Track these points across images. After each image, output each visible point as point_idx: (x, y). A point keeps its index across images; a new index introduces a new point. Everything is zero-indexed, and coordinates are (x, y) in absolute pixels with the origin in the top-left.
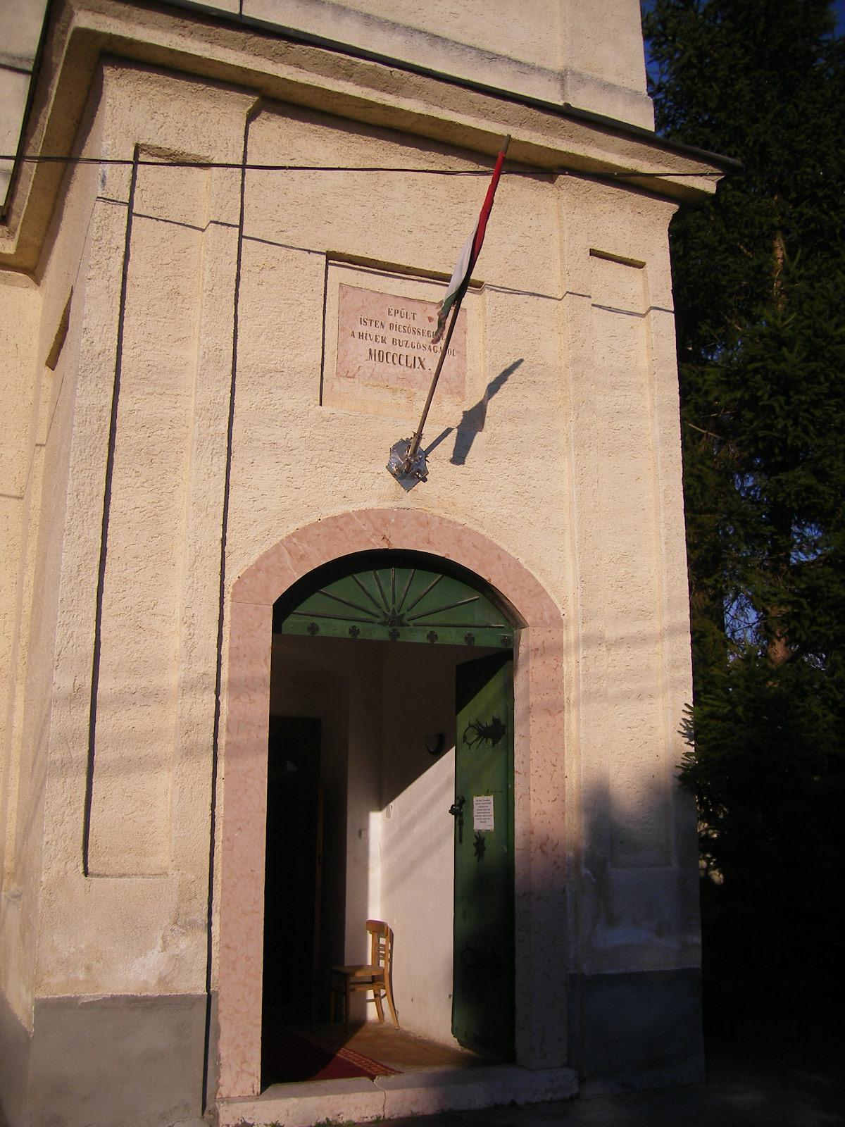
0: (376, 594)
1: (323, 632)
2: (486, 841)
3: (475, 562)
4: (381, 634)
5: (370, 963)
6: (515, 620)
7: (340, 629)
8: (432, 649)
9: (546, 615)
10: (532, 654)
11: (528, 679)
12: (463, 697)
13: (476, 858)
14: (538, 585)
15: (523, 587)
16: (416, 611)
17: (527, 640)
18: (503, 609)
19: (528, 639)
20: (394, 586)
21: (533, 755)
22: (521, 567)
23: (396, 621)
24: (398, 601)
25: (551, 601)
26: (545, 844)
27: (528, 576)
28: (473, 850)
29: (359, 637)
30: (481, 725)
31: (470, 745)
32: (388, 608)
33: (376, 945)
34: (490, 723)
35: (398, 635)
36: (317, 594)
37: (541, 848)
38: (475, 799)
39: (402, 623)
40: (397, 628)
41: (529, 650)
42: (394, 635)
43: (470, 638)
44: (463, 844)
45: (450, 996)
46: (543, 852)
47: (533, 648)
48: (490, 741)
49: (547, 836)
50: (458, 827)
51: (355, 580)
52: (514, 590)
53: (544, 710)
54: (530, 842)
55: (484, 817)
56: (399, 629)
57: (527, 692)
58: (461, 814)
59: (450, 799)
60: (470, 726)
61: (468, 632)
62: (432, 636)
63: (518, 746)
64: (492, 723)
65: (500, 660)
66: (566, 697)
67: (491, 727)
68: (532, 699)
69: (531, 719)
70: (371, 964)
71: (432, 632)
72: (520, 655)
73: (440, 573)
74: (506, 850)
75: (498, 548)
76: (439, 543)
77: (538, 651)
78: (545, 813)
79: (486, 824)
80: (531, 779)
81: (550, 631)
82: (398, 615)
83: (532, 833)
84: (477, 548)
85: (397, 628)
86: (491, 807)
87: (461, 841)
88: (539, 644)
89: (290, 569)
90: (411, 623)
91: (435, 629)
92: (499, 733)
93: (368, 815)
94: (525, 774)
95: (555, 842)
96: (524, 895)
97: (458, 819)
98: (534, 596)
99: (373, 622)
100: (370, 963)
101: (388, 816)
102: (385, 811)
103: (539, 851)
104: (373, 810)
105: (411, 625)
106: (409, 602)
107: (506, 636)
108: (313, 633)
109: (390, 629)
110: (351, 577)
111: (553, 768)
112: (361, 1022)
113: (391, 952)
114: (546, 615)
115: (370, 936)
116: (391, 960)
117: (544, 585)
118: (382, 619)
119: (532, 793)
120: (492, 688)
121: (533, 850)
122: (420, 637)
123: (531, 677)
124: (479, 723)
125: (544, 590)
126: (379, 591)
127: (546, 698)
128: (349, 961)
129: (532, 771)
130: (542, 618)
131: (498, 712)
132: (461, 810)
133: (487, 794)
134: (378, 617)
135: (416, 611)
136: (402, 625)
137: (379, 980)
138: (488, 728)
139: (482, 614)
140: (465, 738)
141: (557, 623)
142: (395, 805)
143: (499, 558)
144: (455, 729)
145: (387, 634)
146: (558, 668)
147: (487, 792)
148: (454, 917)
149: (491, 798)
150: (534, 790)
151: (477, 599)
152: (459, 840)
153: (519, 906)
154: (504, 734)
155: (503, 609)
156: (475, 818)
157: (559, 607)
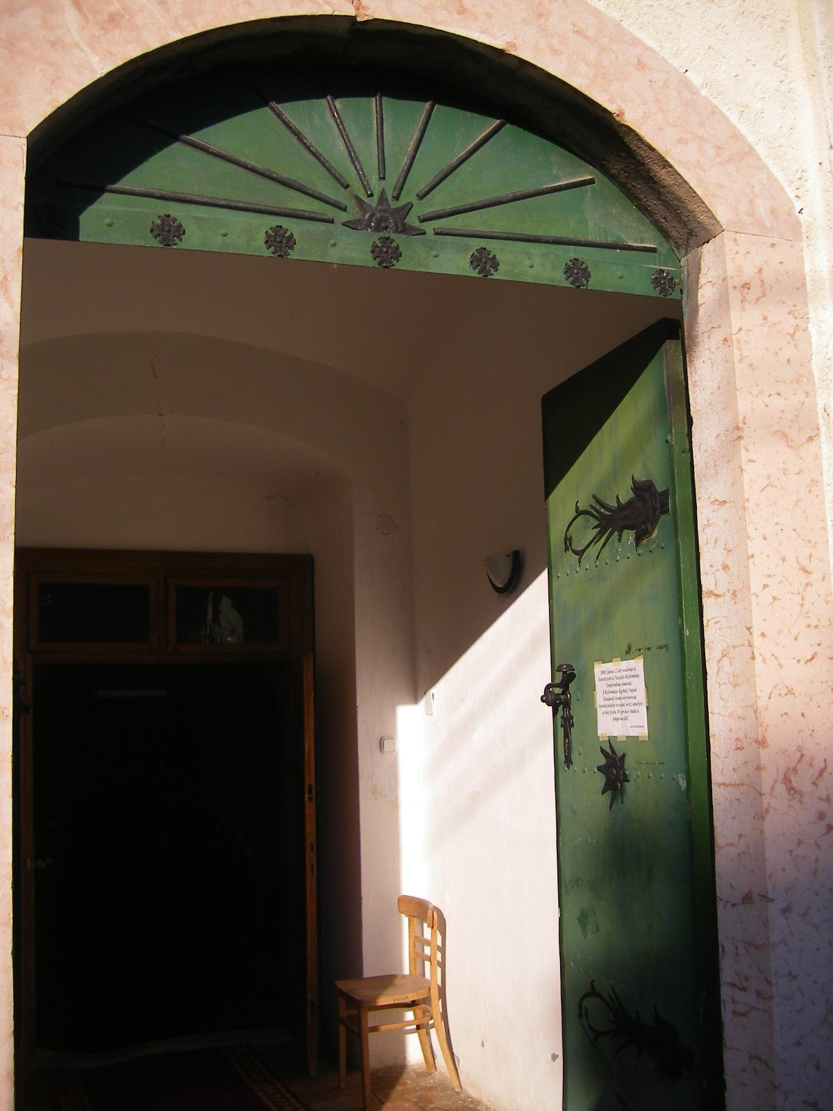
0: (336, 152)
1: (193, 239)
2: (629, 763)
3: (582, 68)
4: (354, 249)
5: (406, 971)
6: (685, 225)
7: (245, 235)
8: (482, 291)
9: (762, 207)
10: (735, 297)
11: (722, 371)
12: (560, 453)
13: (606, 799)
14: (736, 136)
15: (701, 138)
16: (441, 200)
17: (716, 269)
18: (653, 203)
19: (724, 262)
20: (381, 137)
21: (754, 546)
22: (694, 92)
23: (389, 221)
24: (393, 175)
25: (770, 174)
26: (795, 770)
27: (713, 113)
28: (600, 780)
29: (294, 255)
30: (603, 506)
31: (580, 554)
32: (366, 187)
33: (418, 941)
34: (625, 495)
35: (397, 254)
36: (176, 146)
37: (786, 780)
38: (599, 669)
39: (404, 225)
40: (393, 236)
41: (726, 288)
42: (386, 254)
43: (576, 271)
44: (575, 767)
45: (554, 1057)
46: (791, 789)
47: (738, 282)
48: (629, 536)
49: (800, 749)
50: (561, 731)
51: (279, 115)
52: (681, 141)
53: (774, 433)
54: (759, 768)
55: (623, 705)
56: (400, 240)
57: (728, 389)
58: (567, 704)
59: (541, 674)
60: (579, 513)
61: (573, 256)
62: (484, 261)
63: (708, 530)
64: (632, 495)
65: (655, 335)
66: (820, 406)
67: (630, 503)
68: (743, 405)
69: (744, 456)
70: (408, 974)
71: (482, 250)
72: (702, 311)
73: (494, 115)
74: (683, 784)
75: (635, 42)
76: (489, 16)
77: (750, 289)
78: (790, 692)
79: (628, 723)
80: (754, 605)
81: (773, 245)
82: (395, 205)
83: (762, 743)
84: (586, 37)
85: (393, 236)
86: (639, 684)
87: (568, 761)
88: (749, 273)
89: (77, 45)
90: (429, 227)
91: (493, 246)
92: (658, 513)
93: (394, 712)
94: (734, 594)
95: (819, 764)
96: (747, 898)
97: (560, 713)
98: (730, 160)
99: (332, 222)
100: (406, 971)
101: (429, 713)
102: (422, 703)
103: (781, 788)
104: (404, 703)
105: (430, 232)
106: (420, 178)
107: (662, 271)
108: (167, 243)
109: (375, 238)
110: (267, 109)
111: (803, 578)
112: (394, 1073)
113: (443, 949)
114: (762, 207)
115: (405, 920)
116: (442, 965)
117: (751, 139)
118: (353, 213)
119: (757, 641)
120: (632, 412)
121: (766, 789)
122: (454, 261)
123: (736, 351)
124: (598, 501)
125: (751, 148)
126: (342, 147)
127: (776, 402)
128: (370, 969)
129: (755, 586)
130: (752, 215)
131: (649, 467)
132: (565, 694)
133: (628, 653)
134: (345, 209)
135: (441, 200)
136: (406, 230)
137: (428, 1005)
138: (621, 508)
139: (601, 215)
140: (568, 541)
141: (787, 226)
142: (443, 689)
143: (641, 66)
144: (546, 528)
145: (369, 249)
146: (797, 334)
147: (628, 652)
148: (560, 920)
149: (638, 664)
150: (763, 635)
151: (591, 182)
152: (564, 757)
153: (729, 925)
154: (666, 511)
155: (653, 203)
156: (600, 711)
157: (791, 192)
